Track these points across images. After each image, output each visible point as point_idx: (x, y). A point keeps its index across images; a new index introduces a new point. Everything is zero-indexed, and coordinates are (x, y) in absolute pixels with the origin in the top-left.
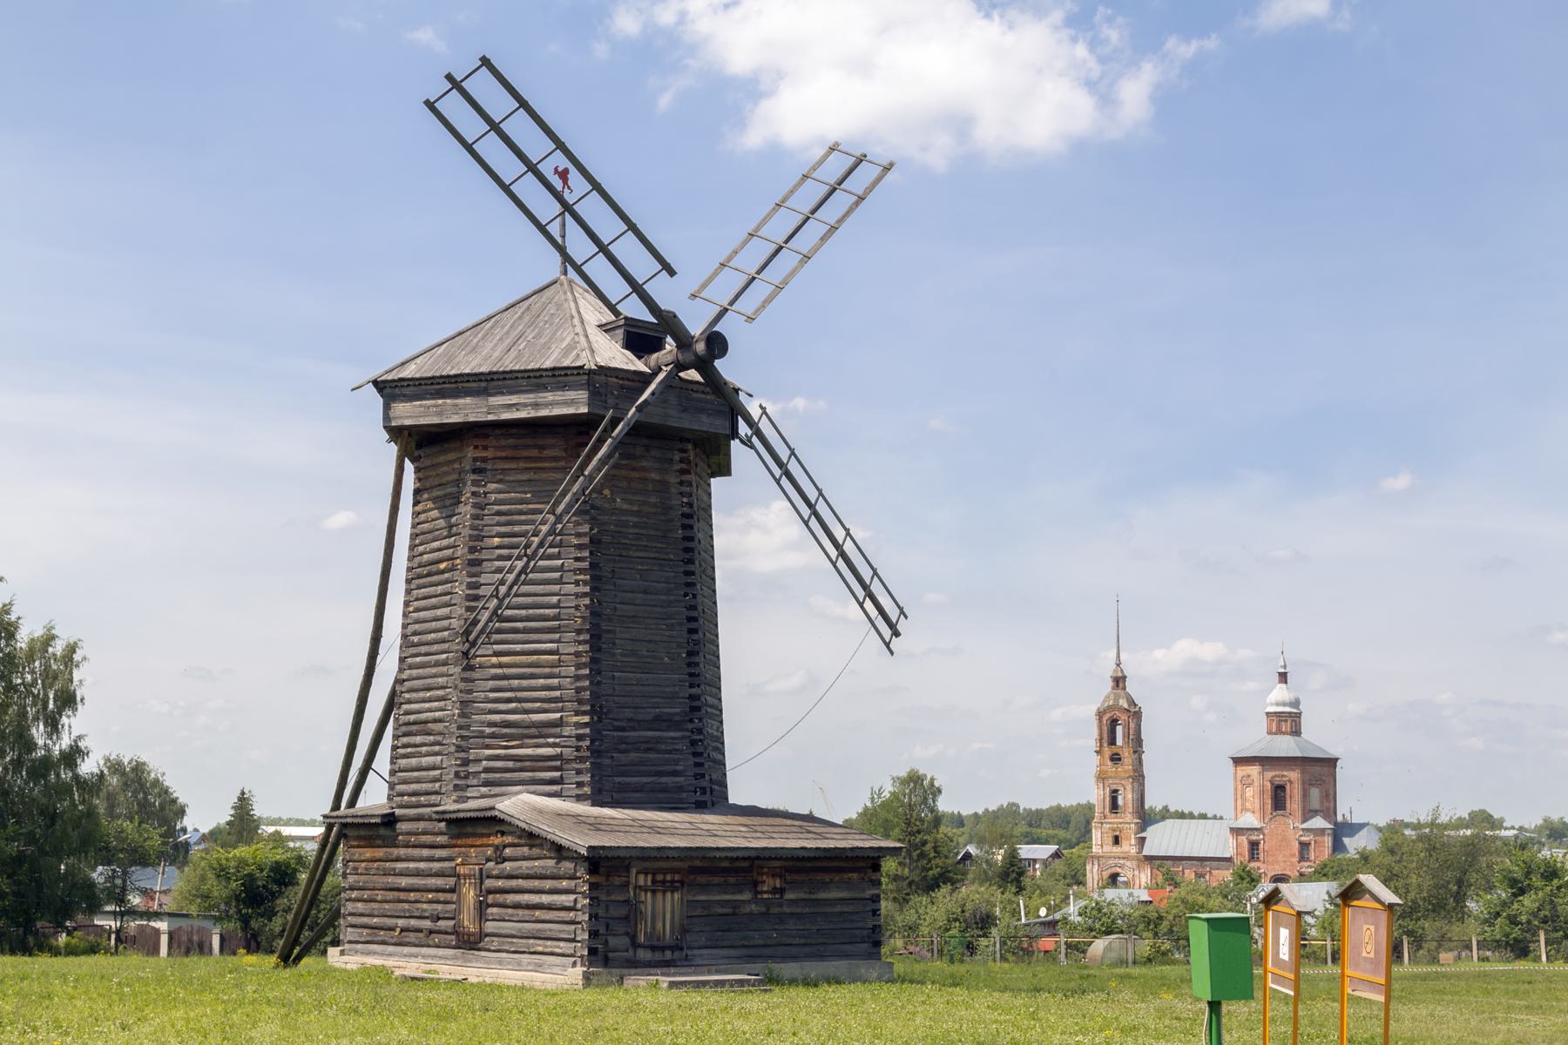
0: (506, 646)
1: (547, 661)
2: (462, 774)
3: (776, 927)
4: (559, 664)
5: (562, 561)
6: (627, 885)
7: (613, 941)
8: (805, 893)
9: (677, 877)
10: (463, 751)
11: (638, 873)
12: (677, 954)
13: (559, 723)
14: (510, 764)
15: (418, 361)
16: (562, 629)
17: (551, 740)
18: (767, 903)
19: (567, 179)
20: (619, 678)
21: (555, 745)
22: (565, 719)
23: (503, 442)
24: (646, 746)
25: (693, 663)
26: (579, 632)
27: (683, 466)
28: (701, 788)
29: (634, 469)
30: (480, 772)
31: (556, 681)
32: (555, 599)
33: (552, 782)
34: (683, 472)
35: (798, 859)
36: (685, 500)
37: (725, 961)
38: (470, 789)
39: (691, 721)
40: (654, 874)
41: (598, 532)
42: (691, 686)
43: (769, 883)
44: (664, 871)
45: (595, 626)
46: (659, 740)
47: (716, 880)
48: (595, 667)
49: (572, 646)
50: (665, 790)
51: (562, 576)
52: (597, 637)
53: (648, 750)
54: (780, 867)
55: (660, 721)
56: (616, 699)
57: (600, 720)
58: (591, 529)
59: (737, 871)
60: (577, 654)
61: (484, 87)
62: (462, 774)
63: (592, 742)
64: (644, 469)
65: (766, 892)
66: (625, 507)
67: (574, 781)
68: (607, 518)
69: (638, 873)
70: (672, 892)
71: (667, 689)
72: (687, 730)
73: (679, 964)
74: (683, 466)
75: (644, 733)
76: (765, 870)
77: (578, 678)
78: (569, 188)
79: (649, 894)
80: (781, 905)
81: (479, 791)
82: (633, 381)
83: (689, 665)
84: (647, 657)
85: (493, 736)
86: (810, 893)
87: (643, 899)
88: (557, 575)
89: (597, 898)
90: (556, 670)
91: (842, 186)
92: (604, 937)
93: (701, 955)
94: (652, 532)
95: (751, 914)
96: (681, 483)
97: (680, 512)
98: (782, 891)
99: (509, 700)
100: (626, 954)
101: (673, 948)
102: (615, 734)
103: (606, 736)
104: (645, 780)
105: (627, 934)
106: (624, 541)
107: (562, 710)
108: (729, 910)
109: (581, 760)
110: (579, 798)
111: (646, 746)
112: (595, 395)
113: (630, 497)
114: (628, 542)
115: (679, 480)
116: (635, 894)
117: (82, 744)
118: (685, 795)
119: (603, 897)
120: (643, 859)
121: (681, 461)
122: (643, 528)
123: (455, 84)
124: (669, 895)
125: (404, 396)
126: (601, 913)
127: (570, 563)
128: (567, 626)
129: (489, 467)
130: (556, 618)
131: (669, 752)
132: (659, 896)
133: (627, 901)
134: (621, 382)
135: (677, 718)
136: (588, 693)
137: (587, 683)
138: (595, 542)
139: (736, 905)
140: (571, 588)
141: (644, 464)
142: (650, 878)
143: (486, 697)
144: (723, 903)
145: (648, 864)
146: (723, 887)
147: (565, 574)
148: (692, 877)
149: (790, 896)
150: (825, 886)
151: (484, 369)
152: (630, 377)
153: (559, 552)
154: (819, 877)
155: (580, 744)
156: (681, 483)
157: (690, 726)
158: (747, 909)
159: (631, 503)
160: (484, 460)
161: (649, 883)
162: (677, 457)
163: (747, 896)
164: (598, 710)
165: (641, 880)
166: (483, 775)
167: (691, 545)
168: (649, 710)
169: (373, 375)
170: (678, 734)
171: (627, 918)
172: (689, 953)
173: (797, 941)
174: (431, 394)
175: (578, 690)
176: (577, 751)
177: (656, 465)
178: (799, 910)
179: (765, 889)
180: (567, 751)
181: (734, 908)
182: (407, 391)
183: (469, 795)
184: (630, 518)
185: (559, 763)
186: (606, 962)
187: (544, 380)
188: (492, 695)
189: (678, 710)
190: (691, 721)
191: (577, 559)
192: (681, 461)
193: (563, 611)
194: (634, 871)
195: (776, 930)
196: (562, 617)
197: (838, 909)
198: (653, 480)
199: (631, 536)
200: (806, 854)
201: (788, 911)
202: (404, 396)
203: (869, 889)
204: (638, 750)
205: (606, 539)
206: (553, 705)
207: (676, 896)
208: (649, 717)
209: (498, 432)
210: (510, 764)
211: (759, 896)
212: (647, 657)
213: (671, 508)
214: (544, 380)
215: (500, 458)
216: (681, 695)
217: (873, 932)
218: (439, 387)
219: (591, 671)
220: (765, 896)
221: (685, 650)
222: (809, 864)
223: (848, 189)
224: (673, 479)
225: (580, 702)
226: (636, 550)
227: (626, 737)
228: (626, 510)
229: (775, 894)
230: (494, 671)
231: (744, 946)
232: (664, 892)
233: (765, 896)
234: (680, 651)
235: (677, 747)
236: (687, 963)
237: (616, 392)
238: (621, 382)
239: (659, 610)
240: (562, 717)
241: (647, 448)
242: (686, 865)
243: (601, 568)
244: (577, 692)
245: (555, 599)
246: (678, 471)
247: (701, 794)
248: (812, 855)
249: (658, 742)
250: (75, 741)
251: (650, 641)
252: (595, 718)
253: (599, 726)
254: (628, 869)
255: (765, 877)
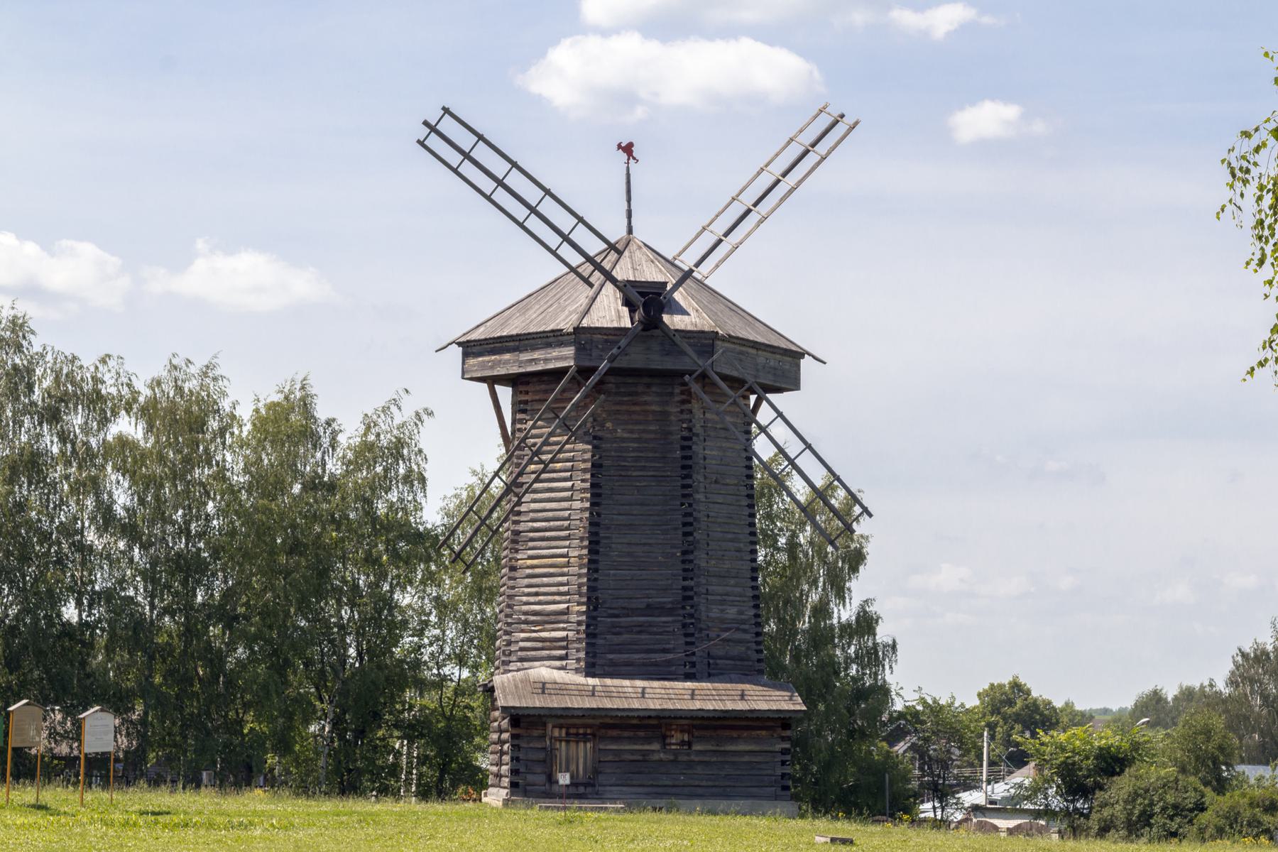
0: (539, 551)
1: (561, 563)
2: (507, 653)
3: (685, 771)
4: (568, 565)
5: (571, 483)
6: (544, 736)
7: (530, 778)
8: (712, 745)
9: (589, 731)
10: (508, 634)
11: (554, 727)
12: (589, 789)
13: (566, 612)
14: (539, 645)
15: (488, 324)
16: (572, 537)
17: (562, 625)
18: (675, 753)
19: (632, 151)
20: (614, 575)
21: (564, 629)
22: (570, 608)
23: (538, 388)
24: (638, 629)
25: (687, 560)
26: (582, 539)
27: (684, 397)
28: (689, 662)
29: (635, 404)
30: (517, 651)
31: (565, 578)
32: (566, 513)
33: (560, 658)
34: (683, 402)
35: (697, 718)
36: (685, 425)
37: (633, 796)
38: (511, 664)
39: (683, 608)
40: (568, 729)
41: (600, 458)
42: (685, 579)
43: (676, 737)
44: (575, 726)
45: (592, 534)
46: (651, 625)
47: (626, 734)
48: (593, 566)
49: (577, 551)
50: (656, 664)
51: (572, 495)
52: (595, 544)
53: (640, 632)
54: (688, 725)
55: (650, 609)
56: (610, 592)
57: (595, 609)
58: (593, 456)
59: (646, 727)
60: (580, 557)
61: (448, 126)
62: (507, 653)
63: (588, 626)
64: (646, 403)
65: (674, 744)
66: (625, 435)
67: (575, 657)
68: (609, 445)
69: (554, 727)
70: (585, 742)
71: (660, 583)
72: (679, 615)
73: (590, 796)
74: (684, 397)
75: (635, 619)
76: (674, 727)
77: (580, 576)
78: (634, 158)
79: (563, 744)
80: (688, 755)
81: (516, 665)
82: (615, 335)
83: (683, 562)
84: (642, 557)
85: (526, 622)
86: (718, 745)
87: (558, 746)
88: (568, 494)
89: (518, 746)
90: (565, 570)
91: (768, 168)
92: (524, 775)
93: (611, 791)
94: (650, 455)
95: (661, 761)
96: (682, 412)
97: (679, 436)
98: (689, 744)
99: (537, 594)
100: (544, 788)
101: (586, 785)
102: (609, 620)
103: (600, 621)
104: (636, 656)
105: (545, 773)
106: (623, 464)
107: (569, 602)
108: (640, 758)
109: (579, 641)
110: (577, 671)
111: (638, 629)
112: (581, 350)
113: (630, 427)
114: (627, 464)
115: (679, 410)
116: (551, 742)
117: (871, 609)
118: (674, 668)
119: (523, 745)
120: (557, 716)
121: (682, 393)
122: (642, 452)
123: (433, 129)
124: (581, 745)
125: (473, 353)
126: (521, 756)
127: (579, 484)
128: (574, 535)
129: (529, 408)
130: (567, 528)
131: (660, 634)
132: (573, 745)
133: (544, 749)
134: (605, 337)
135: (670, 606)
136: (585, 588)
137: (585, 580)
138: (596, 467)
139: (645, 753)
140: (577, 505)
141: (646, 398)
142: (564, 731)
143: (523, 592)
144: (632, 752)
145: (562, 721)
146: (631, 740)
147: (576, 493)
148: (603, 731)
149: (697, 747)
150: (733, 740)
151: (514, 332)
152: (613, 333)
153: (571, 475)
154: (727, 733)
155: (579, 628)
156: (682, 412)
157: (681, 612)
158: (656, 757)
159: (632, 432)
160: (526, 402)
161: (563, 734)
162: (677, 390)
163: (656, 746)
164: (594, 602)
165: (556, 733)
166: (519, 653)
167: (689, 462)
168: (642, 600)
169: (456, 334)
170: (670, 619)
171: (544, 761)
172: (600, 788)
173: (704, 783)
174: (488, 352)
175: (580, 586)
176: (578, 633)
177: (657, 399)
178: (706, 759)
179: (674, 741)
180: (571, 634)
181: (644, 755)
182: (475, 350)
183: (511, 669)
184: (632, 445)
185: (565, 643)
186: (526, 794)
187: (551, 340)
188: (527, 590)
189: (670, 600)
190: (683, 608)
191: (583, 481)
192: (682, 393)
193: (573, 522)
194: (550, 726)
195: (684, 774)
196: (572, 527)
197: (746, 759)
198: (654, 412)
199: (629, 459)
200: (706, 715)
201: (697, 759)
202: (473, 353)
203: (779, 744)
204: (631, 632)
205: (606, 463)
206: (564, 598)
207: (588, 745)
208: (643, 606)
209: (535, 379)
210: (539, 645)
211: (668, 747)
212: (642, 557)
213: (671, 433)
214: (551, 340)
215: (536, 401)
216: (674, 587)
217: (782, 779)
218: (492, 346)
219: (589, 570)
220: (673, 747)
221: (679, 550)
222: (715, 723)
223: (771, 171)
224: (673, 409)
225: (580, 595)
226: (634, 471)
227: (620, 622)
228: (628, 438)
229: (683, 746)
230: (529, 571)
231: (652, 786)
232: (577, 742)
233: (673, 747)
234: (674, 551)
235: (668, 629)
236: (595, 796)
237: (600, 346)
238: (605, 337)
239: (656, 518)
240: (568, 607)
241: (649, 386)
242: (598, 722)
243: (601, 487)
244: (579, 587)
245: (566, 513)
246: (678, 402)
247: (690, 667)
248: (711, 715)
249: (650, 626)
250: (862, 607)
251: (645, 544)
252: (591, 607)
253: (595, 614)
254: (545, 725)
255: (673, 733)
